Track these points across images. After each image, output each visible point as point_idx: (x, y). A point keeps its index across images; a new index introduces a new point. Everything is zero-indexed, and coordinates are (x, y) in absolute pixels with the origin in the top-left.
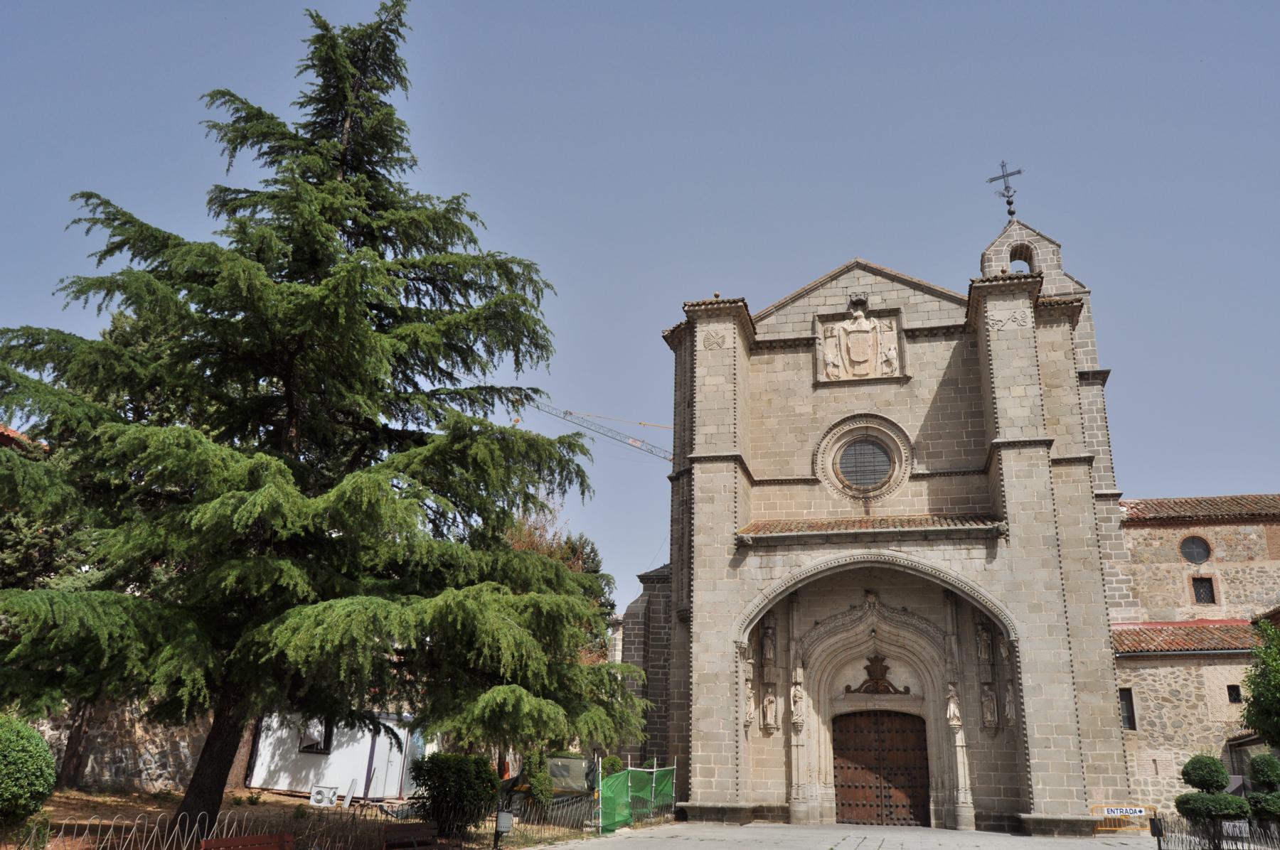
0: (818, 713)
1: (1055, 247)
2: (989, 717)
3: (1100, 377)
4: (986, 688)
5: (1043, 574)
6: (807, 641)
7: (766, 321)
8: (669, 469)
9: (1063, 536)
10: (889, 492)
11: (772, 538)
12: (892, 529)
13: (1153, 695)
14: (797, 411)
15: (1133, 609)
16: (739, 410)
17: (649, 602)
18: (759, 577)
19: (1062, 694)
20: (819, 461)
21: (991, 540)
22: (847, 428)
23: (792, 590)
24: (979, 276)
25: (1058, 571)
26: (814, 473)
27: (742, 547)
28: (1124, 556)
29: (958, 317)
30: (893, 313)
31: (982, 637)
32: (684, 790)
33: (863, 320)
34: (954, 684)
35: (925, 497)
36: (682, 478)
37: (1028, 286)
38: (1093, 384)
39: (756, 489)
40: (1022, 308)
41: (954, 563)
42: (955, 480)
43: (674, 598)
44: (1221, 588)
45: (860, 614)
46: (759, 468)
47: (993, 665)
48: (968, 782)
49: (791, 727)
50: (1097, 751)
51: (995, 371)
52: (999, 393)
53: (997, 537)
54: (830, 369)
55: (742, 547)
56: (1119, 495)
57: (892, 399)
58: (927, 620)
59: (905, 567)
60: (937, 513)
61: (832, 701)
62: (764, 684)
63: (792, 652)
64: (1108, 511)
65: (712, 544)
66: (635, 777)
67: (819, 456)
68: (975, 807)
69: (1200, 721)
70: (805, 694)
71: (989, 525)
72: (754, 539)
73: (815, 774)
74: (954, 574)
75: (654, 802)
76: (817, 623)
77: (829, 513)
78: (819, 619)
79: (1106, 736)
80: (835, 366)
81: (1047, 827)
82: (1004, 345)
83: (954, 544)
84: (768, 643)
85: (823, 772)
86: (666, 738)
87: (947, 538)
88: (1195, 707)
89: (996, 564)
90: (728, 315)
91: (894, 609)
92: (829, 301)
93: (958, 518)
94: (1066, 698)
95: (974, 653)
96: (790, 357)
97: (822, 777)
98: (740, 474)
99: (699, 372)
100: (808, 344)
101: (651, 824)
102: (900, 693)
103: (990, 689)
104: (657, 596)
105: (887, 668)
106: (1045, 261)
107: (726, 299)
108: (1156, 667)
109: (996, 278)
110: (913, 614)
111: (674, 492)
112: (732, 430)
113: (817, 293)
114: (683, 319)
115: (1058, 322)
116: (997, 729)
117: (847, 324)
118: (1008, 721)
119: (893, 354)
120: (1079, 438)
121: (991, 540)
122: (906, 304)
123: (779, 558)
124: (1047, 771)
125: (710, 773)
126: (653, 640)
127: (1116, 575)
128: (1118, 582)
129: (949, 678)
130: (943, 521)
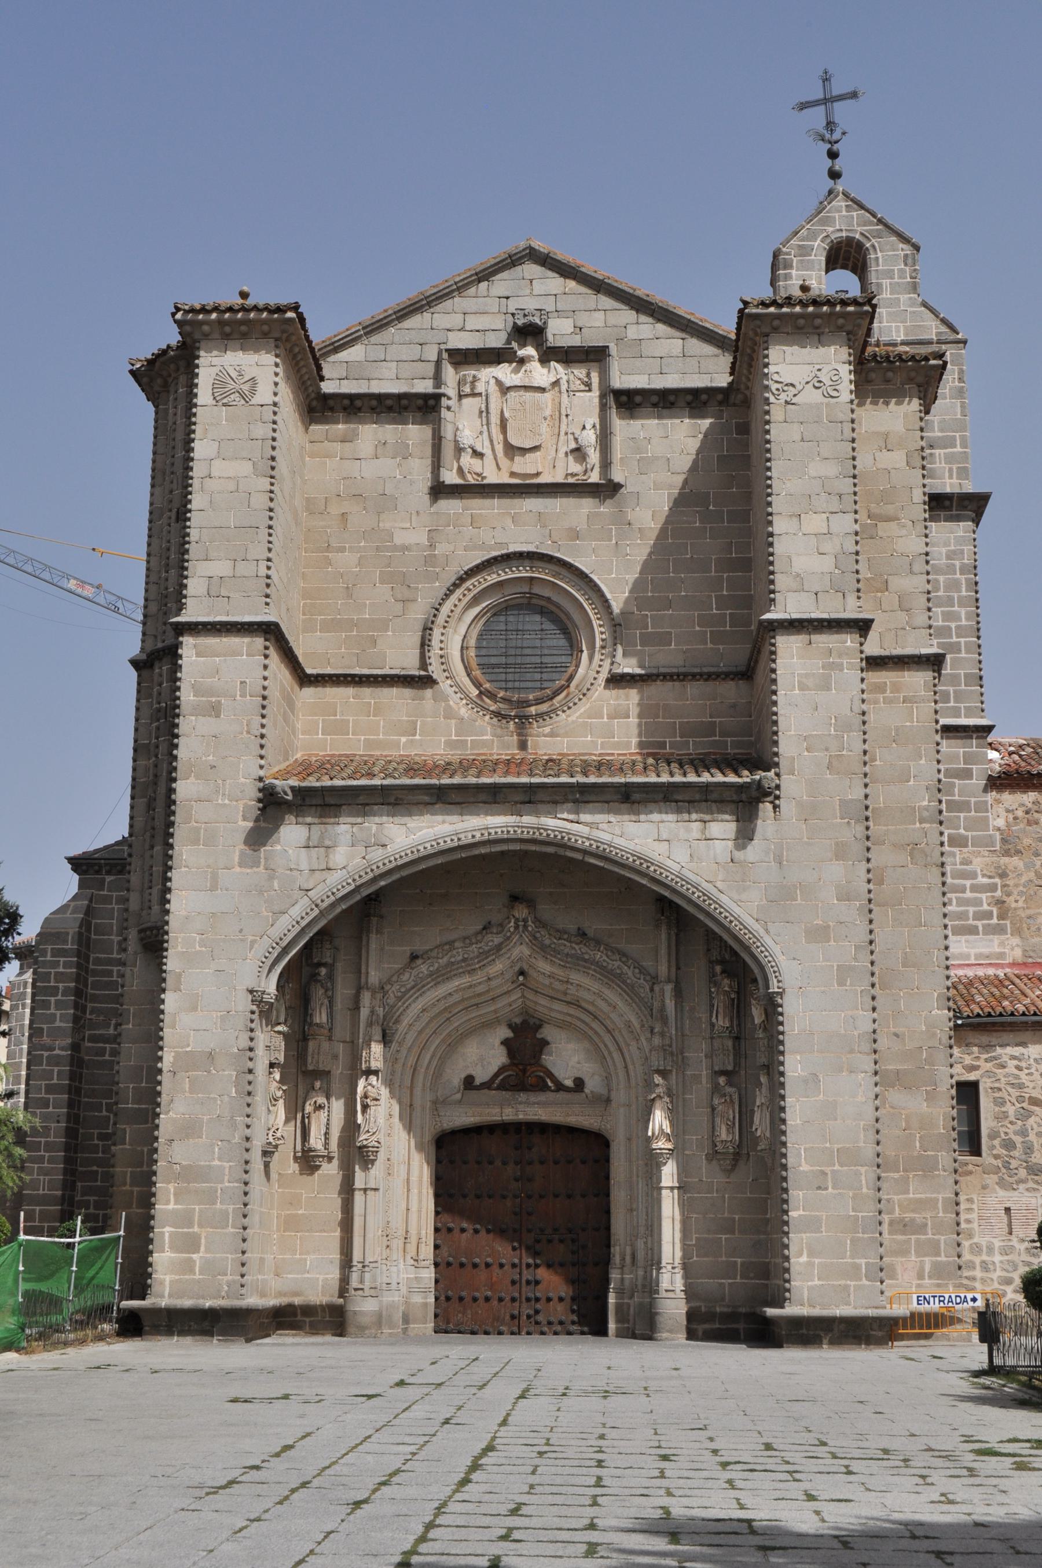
0: (409, 1127)
1: (908, 250)
2: (724, 1135)
3: (971, 506)
4: (722, 1080)
5: (835, 871)
6: (393, 991)
7: (343, 355)
8: (132, 644)
9: (880, 797)
10: (566, 707)
11: (333, 789)
12: (564, 779)
13: (1015, 1093)
14: (398, 540)
15: (996, 939)
16: (278, 530)
17: (89, 911)
18: (304, 866)
19: (855, 1092)
20: (435, 643)
21: (746, 804)
22: (492, 578)
23: (365, 892)
24: (767, 294)
26: (424, 665)
27: (273, 806)
28: (989, 842)
29: (713, 371)
30: (593, 356)
31: (718, 982)
32: (138, 1280)
33: (535, 366)
34: (663, 1073)
35: (634, 720)
36: (157, 663)
37: (847, 320)
38: (958, 519)
39: (309, 693)
40: (833, 362)
42: (692, 689)
43: (134, 905)
45: (497, 940)
46: (314, 650)
47: (737, 1039)
48: (679, 1254)
49: (355, 1153)
50: (910, 1193)
52: (779, 525)
53: (758, 800)
54: (466, 460)
55: (273, 806)
56: (988, 729)
57: (581, 523)
58: (623, 954)
59: (585, 852)
60: (654, 751)
61: (438, 1104)
62: (306, 1073)
63: (364, 1012)
64: (968, 759)
65: (213, 794)
66: (32, 1254)
67: (437, 633)
68: (688, 1299)
70: (384, 1092)
71: (746, 777)
72: (296, 791)
73: (397, 1243)
74: (675, 867)
75: (73, 1303)
76: (414, 957)
77: (449, 744)
78: (419, 947)
79: (927, 1168)
80: (477, 454)
81: (811, 1332)
82: (795, 432)
83: (679, 811)
84: (318, 993)
85: (414, 1240)
86: (108, 1177)
87: (666, 799)
89: (753, 851)
90: (265, 335)
91: (561, 933)
92: (472, 322)
93: (692, 762)
94: (860, 1098)
95: (704, 1017)
96: (389, 432)
97: (412, 1249)
98: (275, 659)
99: (201, 449)
100: (425, 407)
101: (66, 1344)
102: (567, 1089)
103: (730, 1083)
104: (107, 900)
105: (545, 1043)
106: (890, 274)
107: (261, 303)
108: (1023, 1044)
109: (789, 301)
110: (598, 942)
111: (142, 692)
112: (263, 571)
113: (448, 304)
114: (173, 337)
115: (900, 395)
116: (737, 1156)
117: (504, 372)
118: (756, 1140)
119: (589, 437)
120: (921, 619)
121: (746, 804)
123: (344, 829)
124: (818, 1230)
125: (191, 1244)
126: (96, 985)
127: (973, 875)
128: (974, 888)
129: (657, 1062)
130: (663, 766)
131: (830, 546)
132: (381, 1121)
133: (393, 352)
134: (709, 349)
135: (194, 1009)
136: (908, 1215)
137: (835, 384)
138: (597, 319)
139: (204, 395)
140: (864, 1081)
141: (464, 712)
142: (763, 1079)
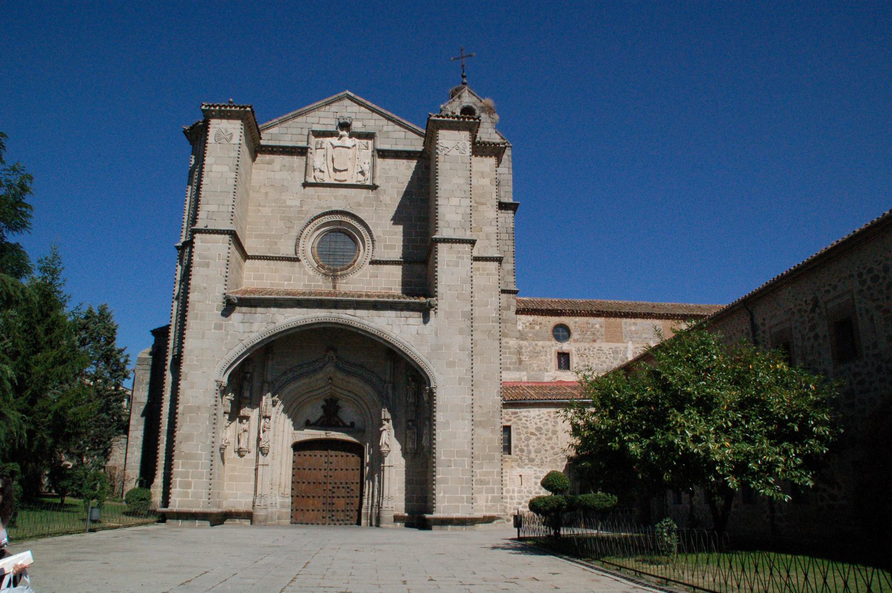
4: (410, 424)
7: (270, 131)
9: (476, 314)
10: (353, 272)
13: (525, 430)
14: (288, 204)
20: (301, 244)
21: (425, 312)
25: (470, 337)
26: (296, 254)
27: (229, 306)
29: (417, 145)
30: (370, 136)
41: (399, 329)
44: (574, 360)
45: (321, 365)
46: (250, 246)
50: (485, 470)
51: (439, 185)
52: (440, 202)
55: (229, 306)
59: (358, 329)
69: (553, 448)
71: (423, 300)
74: (394, 336)
77: (304, 285)
79: (491, 459)
80: (321, 171)
82: (448, 166)
84: (246, 385)
85: (283, 486)
88: (550, 439)
92: (323, 121)
94: (466, 430)
96: (286, 159)
100: (302, 151)
112: (231, 210)
113: (313, 114)
117: (335, 141)
118: (423, 447)
119: (367, 167)
120: (495, 243)
121: (425, 312)
122: (380, 131)
125: (188, 485)
128: (510, 353)
131: (461, 211)
132: (270, 437)
133: (290, 131)
134: (416, 136)
135: (192, 388)
136: (483, 478)
137: (464, 149)
138: (372, 123)
139: (211, 139)
140: (468, 423)
141: (311, 273)
142: (427, 423)
